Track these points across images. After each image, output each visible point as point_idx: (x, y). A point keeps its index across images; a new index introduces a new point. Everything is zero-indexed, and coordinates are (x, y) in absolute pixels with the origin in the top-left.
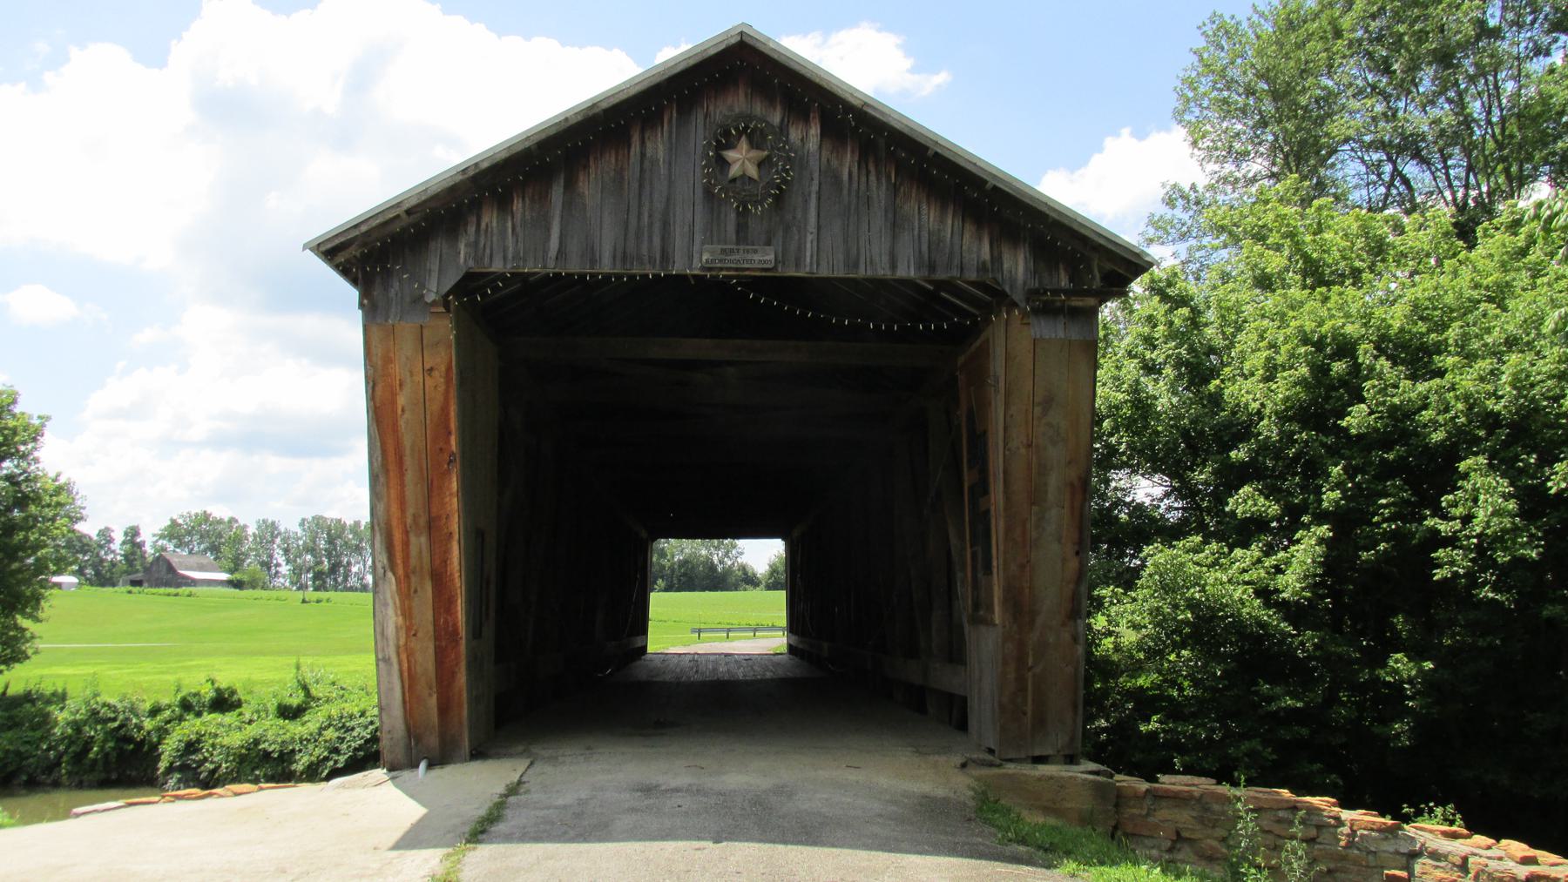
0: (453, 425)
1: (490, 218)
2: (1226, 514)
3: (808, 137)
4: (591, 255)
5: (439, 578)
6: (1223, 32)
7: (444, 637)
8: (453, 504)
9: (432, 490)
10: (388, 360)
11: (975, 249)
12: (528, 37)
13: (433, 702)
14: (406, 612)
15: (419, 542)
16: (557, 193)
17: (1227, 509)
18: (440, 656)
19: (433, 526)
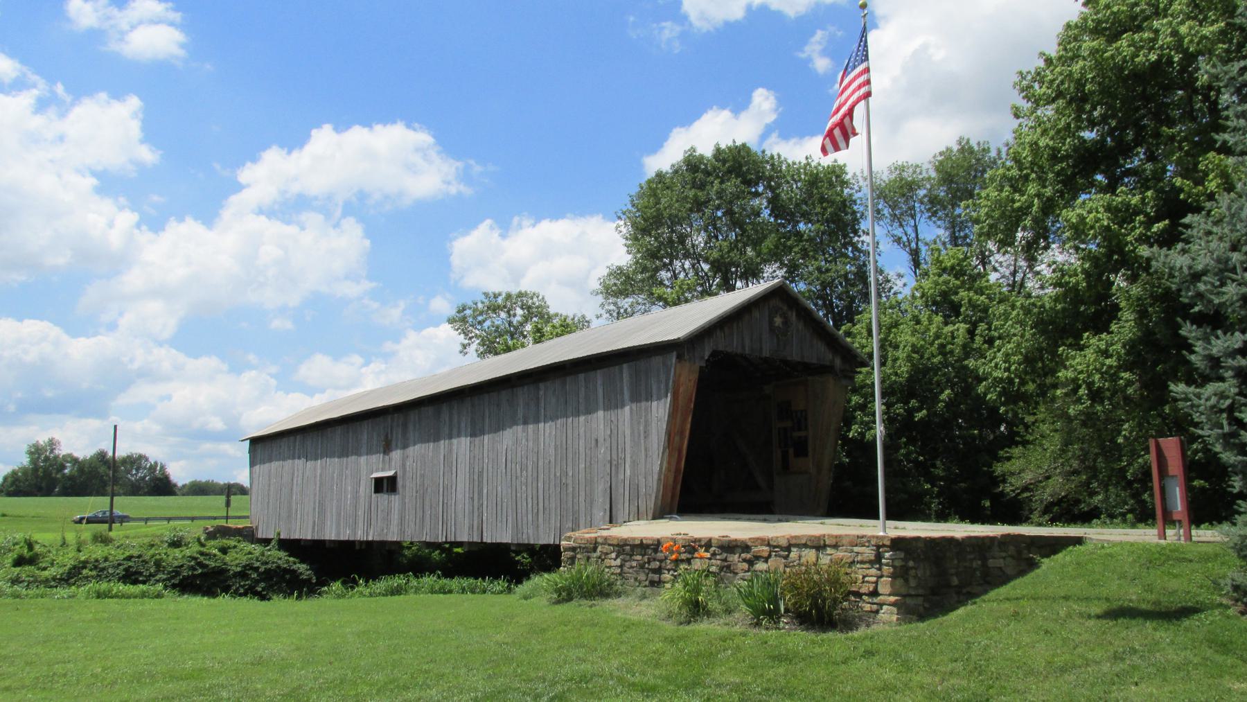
0: (693, 399)
1: (718, 332)
2: (1054, 353)
3: (793, 317)
4: (743, 347)
5: (680, 451)
6: (693, 149)
7: (677, 471)
8: (688, 426)
9: (684, 421)
10: (680, 375)
11: (829, 356)
12: (385, 125)
13: (670, 495)
14: (669, 463)
15: (677, 439)
16: (735, 325)
17: (1082, 342)
18: (675, 478)
19: (682, 433)
